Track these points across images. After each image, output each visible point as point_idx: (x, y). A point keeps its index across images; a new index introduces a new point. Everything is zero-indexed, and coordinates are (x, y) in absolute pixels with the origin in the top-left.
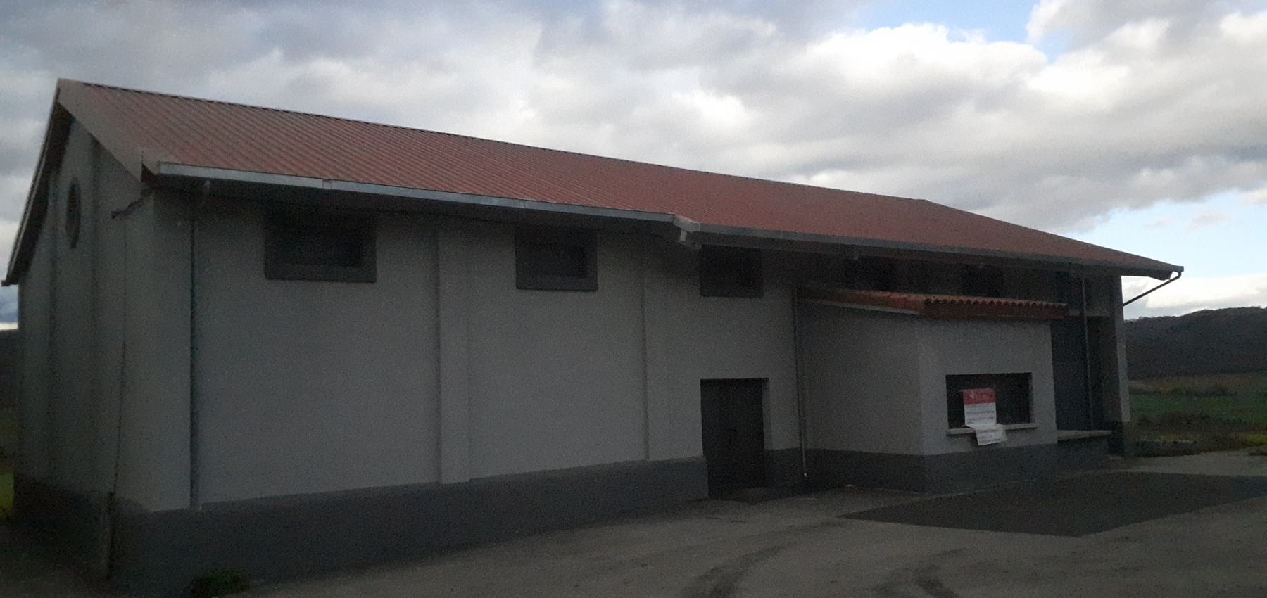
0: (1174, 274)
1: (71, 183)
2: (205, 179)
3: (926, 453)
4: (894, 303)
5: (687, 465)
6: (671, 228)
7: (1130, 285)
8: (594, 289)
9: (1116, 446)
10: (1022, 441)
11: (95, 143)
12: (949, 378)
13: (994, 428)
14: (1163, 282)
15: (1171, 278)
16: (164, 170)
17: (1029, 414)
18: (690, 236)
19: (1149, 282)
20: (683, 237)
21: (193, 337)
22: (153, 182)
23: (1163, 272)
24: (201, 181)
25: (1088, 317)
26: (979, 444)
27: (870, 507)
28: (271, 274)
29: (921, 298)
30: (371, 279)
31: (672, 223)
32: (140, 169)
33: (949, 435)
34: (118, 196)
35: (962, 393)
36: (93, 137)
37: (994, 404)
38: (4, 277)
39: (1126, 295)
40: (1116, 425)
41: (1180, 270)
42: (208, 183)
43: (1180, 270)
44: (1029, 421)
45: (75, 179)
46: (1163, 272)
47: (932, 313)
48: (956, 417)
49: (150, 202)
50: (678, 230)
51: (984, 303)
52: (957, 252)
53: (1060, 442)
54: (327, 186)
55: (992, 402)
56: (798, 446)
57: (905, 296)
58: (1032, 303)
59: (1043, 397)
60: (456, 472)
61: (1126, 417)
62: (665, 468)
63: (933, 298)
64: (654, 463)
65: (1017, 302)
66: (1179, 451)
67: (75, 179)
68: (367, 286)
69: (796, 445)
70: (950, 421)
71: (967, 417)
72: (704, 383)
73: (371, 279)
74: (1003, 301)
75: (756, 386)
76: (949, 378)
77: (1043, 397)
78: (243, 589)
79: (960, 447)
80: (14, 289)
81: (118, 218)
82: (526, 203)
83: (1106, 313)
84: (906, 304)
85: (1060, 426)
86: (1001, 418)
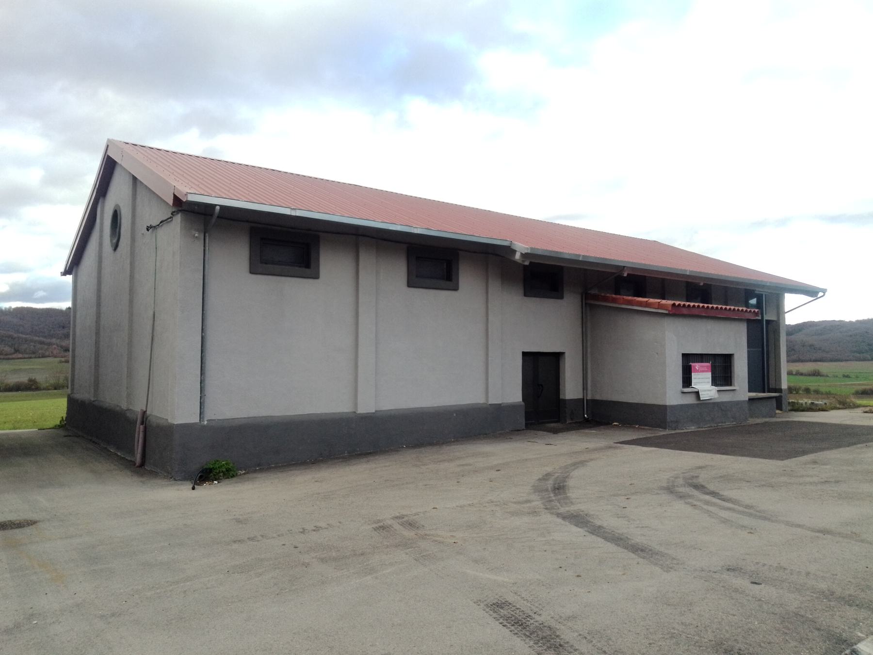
0: (821, 294)
1: (115, 208)
2: (216, 205)
3: (668, 404)
4: (647, 305)
5: (512, 407)
6: (509, 250)
7: (790, 300)
8: (456, 288)
9: (779, 403)
10: (726, 398)
11: (135, 179)
12: (684, 355)
13: (710, 389)
14: (813, 299)
15: (819, 296)
16: (191, 198)
17: (731, 382)
18: (525, 256)
19: (802, 298)
20: (517, 256)
21: (469, 252)
22: (180, 205)
23: (812, 292)
24: (213, 206)
25: (766, 320)
26: (701, 399)
27: (635, 437)
28: (253, 271)
29: (670, 302)
30: (316, 276)
31: (510, 247)
32: (172, 197)
33: (683, 393)
34: (152, 214)
35: (691, 365)
36: (133, 175)
37: (711, 373)
38: (62, 270)
39: (787, 307)
40: (780, 390)
41: (824, 291)
42: (218, 208)
43: (824, 291)
44: (731, 385)
45: (117, 206)
46: (812, 292)
47: (676, 313)
48: (687, 381)
49: (178, 218)
50: (514, 252)
51: (717, 308)
52: (688, 274)
53: (751, 400)
54: (293, 213)
55: (709, 372)
56: (582, 397)
57: (659, 301)
58: (736, 308)
59: (741, 369)
60: (367, 406)
61: (784, 386)
62: (499, 408)
63: (677, 303)
64: (491, 405)
65: (720, 306)
66: (812, 408)
67: (117, 206)
68: (311, 281)
69: (581, 397)
70: (684, 382)
71: (693, 381)
72: (525, 354)
73: (316, 276)
74: (710, 306)
75: (556, 357)
76: (684, 355)
77: (741, 369)
78: (233, 476)
79: (690, 400)
80: (69, 278)
81: (151, 230)
82: (418, 230)
83: (774, 318)
84: (660, 306)
85: (750, 391)
86: (715, 382)
